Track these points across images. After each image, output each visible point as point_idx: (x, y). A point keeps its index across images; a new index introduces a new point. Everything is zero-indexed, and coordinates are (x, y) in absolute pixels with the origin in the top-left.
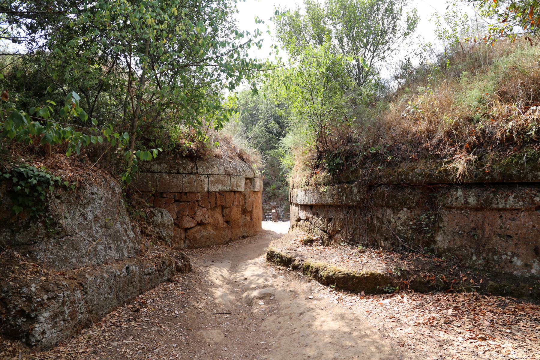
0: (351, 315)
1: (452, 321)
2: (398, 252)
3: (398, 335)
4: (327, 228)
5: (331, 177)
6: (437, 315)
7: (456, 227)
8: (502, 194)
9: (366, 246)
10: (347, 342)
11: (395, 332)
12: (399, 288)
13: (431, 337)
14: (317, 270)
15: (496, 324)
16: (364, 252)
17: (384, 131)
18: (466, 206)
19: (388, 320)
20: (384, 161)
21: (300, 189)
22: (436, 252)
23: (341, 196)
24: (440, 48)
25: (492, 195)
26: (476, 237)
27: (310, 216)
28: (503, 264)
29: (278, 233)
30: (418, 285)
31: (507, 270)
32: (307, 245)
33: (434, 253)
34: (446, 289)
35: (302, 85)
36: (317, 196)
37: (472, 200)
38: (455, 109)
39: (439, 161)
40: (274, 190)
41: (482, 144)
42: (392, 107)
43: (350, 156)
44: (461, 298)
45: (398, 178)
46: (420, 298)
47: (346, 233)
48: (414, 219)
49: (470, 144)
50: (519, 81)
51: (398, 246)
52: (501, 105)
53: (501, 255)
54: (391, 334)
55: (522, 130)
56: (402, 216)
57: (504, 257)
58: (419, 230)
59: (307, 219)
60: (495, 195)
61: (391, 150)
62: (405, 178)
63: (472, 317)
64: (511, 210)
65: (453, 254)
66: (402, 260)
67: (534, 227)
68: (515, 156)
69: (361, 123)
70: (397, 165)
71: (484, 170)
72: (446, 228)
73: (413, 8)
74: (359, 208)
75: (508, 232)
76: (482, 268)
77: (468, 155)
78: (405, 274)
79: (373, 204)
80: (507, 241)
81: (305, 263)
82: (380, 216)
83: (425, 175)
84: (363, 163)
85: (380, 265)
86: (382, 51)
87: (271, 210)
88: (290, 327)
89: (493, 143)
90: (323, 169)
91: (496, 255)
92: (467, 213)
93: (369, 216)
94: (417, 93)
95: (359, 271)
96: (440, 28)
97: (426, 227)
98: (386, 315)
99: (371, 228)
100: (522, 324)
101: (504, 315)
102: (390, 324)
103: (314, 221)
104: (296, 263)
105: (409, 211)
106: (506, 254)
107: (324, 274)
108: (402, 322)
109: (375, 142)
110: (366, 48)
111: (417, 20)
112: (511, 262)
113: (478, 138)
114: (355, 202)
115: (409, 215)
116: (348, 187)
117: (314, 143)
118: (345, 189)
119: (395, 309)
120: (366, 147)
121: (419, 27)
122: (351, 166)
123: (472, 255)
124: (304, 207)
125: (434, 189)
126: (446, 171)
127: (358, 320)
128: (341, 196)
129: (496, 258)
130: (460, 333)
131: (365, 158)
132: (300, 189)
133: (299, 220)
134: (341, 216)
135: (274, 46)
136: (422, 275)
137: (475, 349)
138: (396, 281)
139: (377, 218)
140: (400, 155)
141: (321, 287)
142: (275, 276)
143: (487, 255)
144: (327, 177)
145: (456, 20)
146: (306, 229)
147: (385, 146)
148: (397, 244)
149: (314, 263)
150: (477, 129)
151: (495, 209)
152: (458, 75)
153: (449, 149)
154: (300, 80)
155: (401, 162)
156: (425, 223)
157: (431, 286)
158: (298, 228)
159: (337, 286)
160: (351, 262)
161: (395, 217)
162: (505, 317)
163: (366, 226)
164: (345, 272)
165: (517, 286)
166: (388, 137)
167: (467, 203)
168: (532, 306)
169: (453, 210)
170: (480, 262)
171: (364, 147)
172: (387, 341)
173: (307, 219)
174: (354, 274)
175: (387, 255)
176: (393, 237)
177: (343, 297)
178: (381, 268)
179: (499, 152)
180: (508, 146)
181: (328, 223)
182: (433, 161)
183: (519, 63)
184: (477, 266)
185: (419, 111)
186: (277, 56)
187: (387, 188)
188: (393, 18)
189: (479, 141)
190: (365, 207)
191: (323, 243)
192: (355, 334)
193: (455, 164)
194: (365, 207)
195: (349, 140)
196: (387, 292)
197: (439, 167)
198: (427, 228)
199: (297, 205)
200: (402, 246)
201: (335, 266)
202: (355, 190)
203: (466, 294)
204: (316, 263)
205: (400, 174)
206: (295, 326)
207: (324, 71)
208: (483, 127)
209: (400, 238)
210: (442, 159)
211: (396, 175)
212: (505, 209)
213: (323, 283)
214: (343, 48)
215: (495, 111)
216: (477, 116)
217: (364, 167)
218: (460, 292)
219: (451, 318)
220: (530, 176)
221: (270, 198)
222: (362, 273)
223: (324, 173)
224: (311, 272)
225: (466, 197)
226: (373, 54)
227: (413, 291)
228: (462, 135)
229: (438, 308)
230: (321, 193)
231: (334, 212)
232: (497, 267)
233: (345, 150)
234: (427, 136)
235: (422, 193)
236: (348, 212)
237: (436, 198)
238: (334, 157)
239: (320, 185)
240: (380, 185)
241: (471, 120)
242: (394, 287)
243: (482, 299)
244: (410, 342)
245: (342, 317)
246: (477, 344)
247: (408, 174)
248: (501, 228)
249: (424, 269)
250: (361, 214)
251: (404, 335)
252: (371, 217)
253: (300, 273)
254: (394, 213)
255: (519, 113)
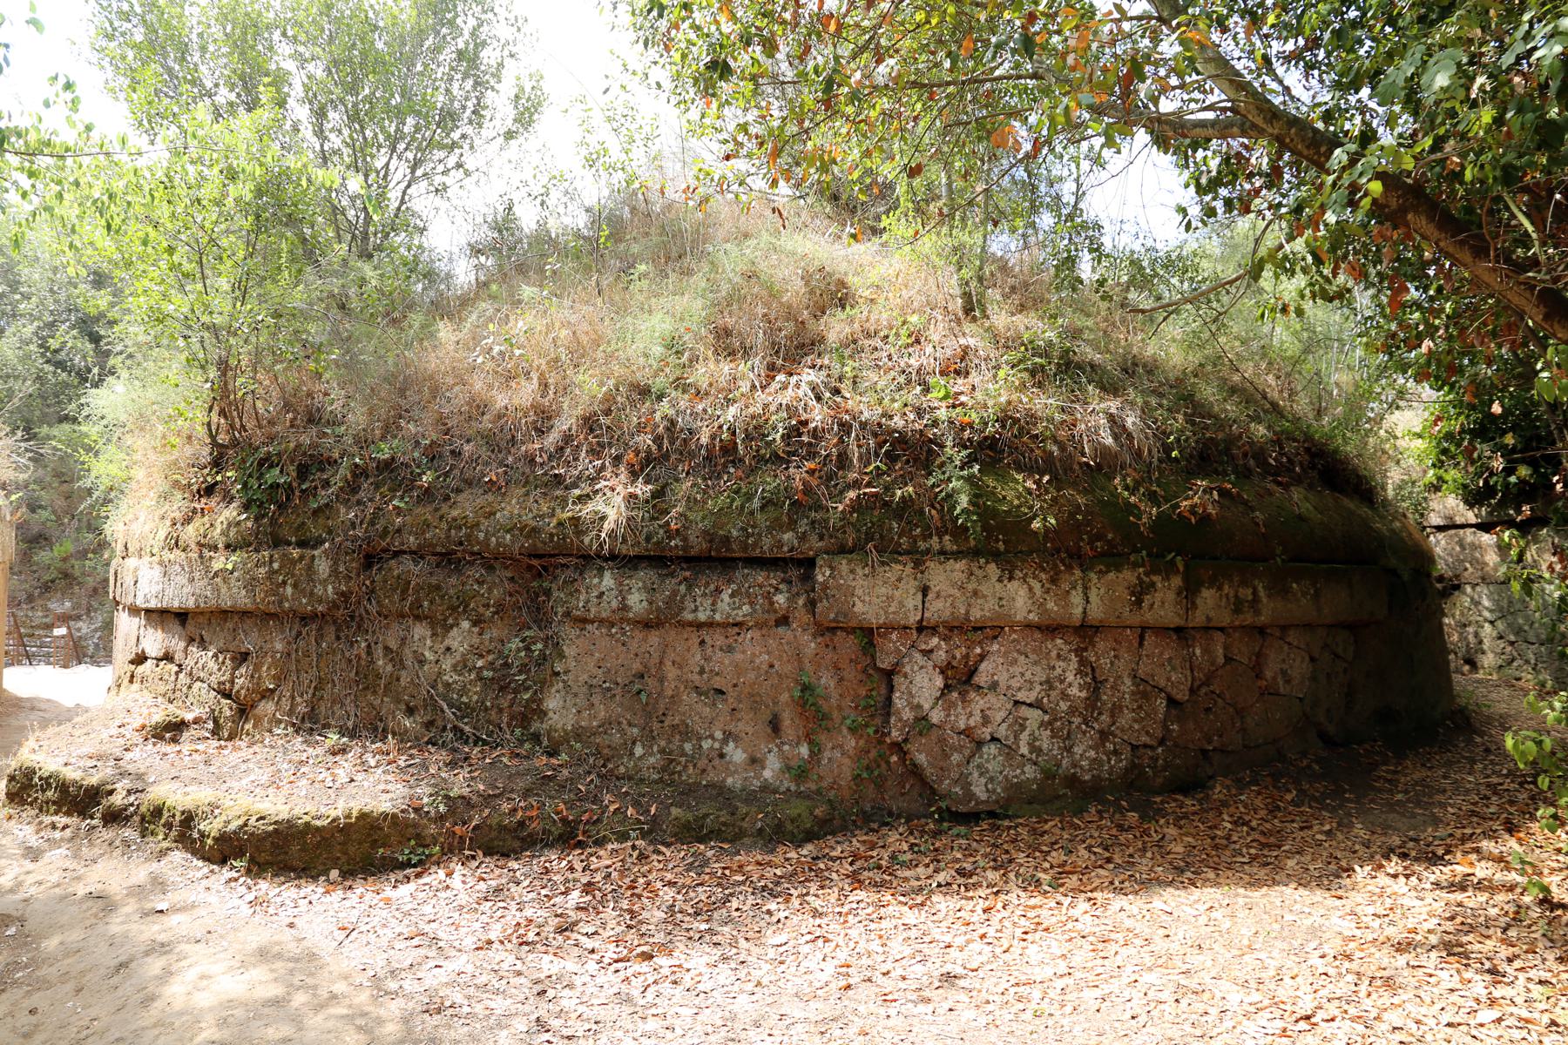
0: (294, 944)
1: (575, 923)
2: (444, 745)
3: (427, 983)
4: (232, 682)
5: (249, 524)
6: (540, 913)
7: (595, 671)
8: (707, 585)
9: (353, 734)
10: (270, 1031)
11: (420, 975)
12: (442, 848)
13: (519, 974)
14: (189, 819)
15: (679, 916)
16: (343, 751)
17: (417, 398)
18: (620, 618)
19: (402, 944)
20: (410, 484)
21: (147, 559)
22: (545, 743)
23: (279, 585)
24: (595, 191)
25: (683, 588)
26: (643, 697)
27: (177, 645)
28: (702, 763)
29: (68, 702)
30: (494, 834)
31: (712, 776)
32: (162, 738)
33: (540, 744)
34: (568, 837)
35: (169, 226)
36: (202, 583)
37: (637, 601)
38: (609, 357)
39: (558, 493)
40: (64, 560)
41: (666, 456)
42: (445, 332)
43: (311, 465)
44: (603, 859)
45: (448, 537)
46: (498, 872)
47: (293, 698)
48: (489, 652)
49: (637, 452)
50: (760, 310)
51: (444, 729)
52: (718, 361)
53: (700, 739)
54: (407, 984)
55: (756, 431)
56: (455, 645)
57: (706, 744)
58: (501, 683)
59: (168, 657)
60: (689, 588)
61: (433, 455)
62: (468, 536)
63: (625, 904)
64: (725, 625)
65: (586, 744)
66: (453, 769)
67: (772, 666)
68: (737, 492)
69: (351, 368)
70: (447, 498)
71: (667, 523)
72: (571, 676)
73: (533, 70)
74: (335, 622)
75: (718, 682)
76: (656, 777)
77: (633, 482)
78: (458, 807)
79: (373, 608)
80: (714, 705)
81: (151, 796)
82: (393, 645)
83: (521, 530)
84: (352, 487)
85: (389, 787)
86: (440, 168)
87: (50, 627)
88: (73, 1019)
89: (692, 455)
90: (228, 499)
91: (689, 740)
92: (624, 634)
93: (363, 645)
94: (520, 302)
95: (323, 810)
96: (590, 139)
97: (520, 672)
98: (398, 930)
99: (366, 679)
100: (735, 904)
101: (700, 889)
102: (406, 955)
103: (190, 662)
104: (118, 800)
105: (476, 630)
106: (712, 737)
107: (211, 827)
108: (441, 944)
109: (390, 429)
110: (394, 150)
111: (539, 104)
112: (722, 756)
113: (658, 440)
114: (320, 601)
115: (476, 640)
116: (302, 558)
117: (201, 416)
118: (294, 562)
119: (427, 909)
120: (363, 442)
121: (546, 122)
122: (315, 496)
123: (634, 743)
124: (159, 616)
125: (545, 568)
126: (575, 520)
127: (312, 956)
128: (279, 585)
129: (688, 747)
130: (593, 951)
131: (359, 473)
132: (147, 559)
133: (140, 659)
134: (279, 646)
135: (62, 81)
136: (506, 807)
137: (624, 987)
138: (432, 829)
139: (386, 648)
140: (457, 472)
141: (200, 867)
142: (33, 854)
143: (669, 742)
144: (238, 524)
145: (633, 127)
146: (162, 688)
147: (417, 443)
148: (440, 723)
149: (175, 795)
150: (658, 416)
151: (690, 624)
152: (627, 268)
153: (586, 465)
154: (162, 212)
155: (458, 491)
156: (517, 663)
157: (530, 835)
158: (136, 686)
159: (252, 860)
160: (304, 782)
161: (437, 646)
162: (702, 893)
163: (352, 675)
164: (280, 818)
165: (733, 814)
166: (428, 418)
167: (624, 608)
168: (759, 858)
169: (589, 627)
170: (652, 760)
171: (357, 441)
172: (394, 1008)
173: (168, 657)
174: (307, 818)
175: (412, 756)
176: (430, 703)
177: (271, 894)
178: (389, 796)
179: (705, 479)
180: (725, 466)
181: (235, 669)
182: (545, 494)
183: (763, 266)
184: (645, 774)
185: (517, 352)
186: (75, 117)
187: (416, 563)
188: (476, 84)
189: (660, 447)
190: (352, 617)
191: (216, 732)
192: (300, 999)
193: (597, 505)
194: (352, 617)
195: (313, 418)
196: (408, 864)
197: (558, 511)
198: (523, 677)
199: (134, 611)
200: (455, 728)
201: (251, 799)
202: (323, 567)
203: (616, 846)
204: (187, 794)
205: (455, 524)
206: (93, 1013)
207: (249, 197)
208: (671, 412)
209: (451, 706)
210: (567, 488)
211: (444, 526)
212: (710, 624)
213: (207, 859)
214: (320, 133)
215: (700, 375)
216: (659, 383)
217: (354, 499)
218: (600, 843)
219: (573, 915)
220: (767, 542)
221: (47, 588)
222: (333, 814)
223: (230, 513)
224: (169, 826)
225: (623, 595)
226: (413, 172)
227: (480, 853)
228: (621, 428)
229: (544, 892)
230: (216, 575)
231: (255, 634)
232: (691, 770)
233: (298, 446)
234: (535, 422)
235: (512, 579)
236: (299, 633)
237: (548, 593)
238: (261, 464)
239: (215, 548)
240: (397, 554)
241: (645, 392)
242: (427, 846)
243: (655, 857)
244: (458, 998)
245: (264, 955)
246: (630, 972)
247: (478, 524)
248: (702, 672)
249: (512, 791)
250: (338, 638)
251: (445, 980)
252: (369, 646)
253: (129, 833)
254: (434, 635)
255: (753, 387)
